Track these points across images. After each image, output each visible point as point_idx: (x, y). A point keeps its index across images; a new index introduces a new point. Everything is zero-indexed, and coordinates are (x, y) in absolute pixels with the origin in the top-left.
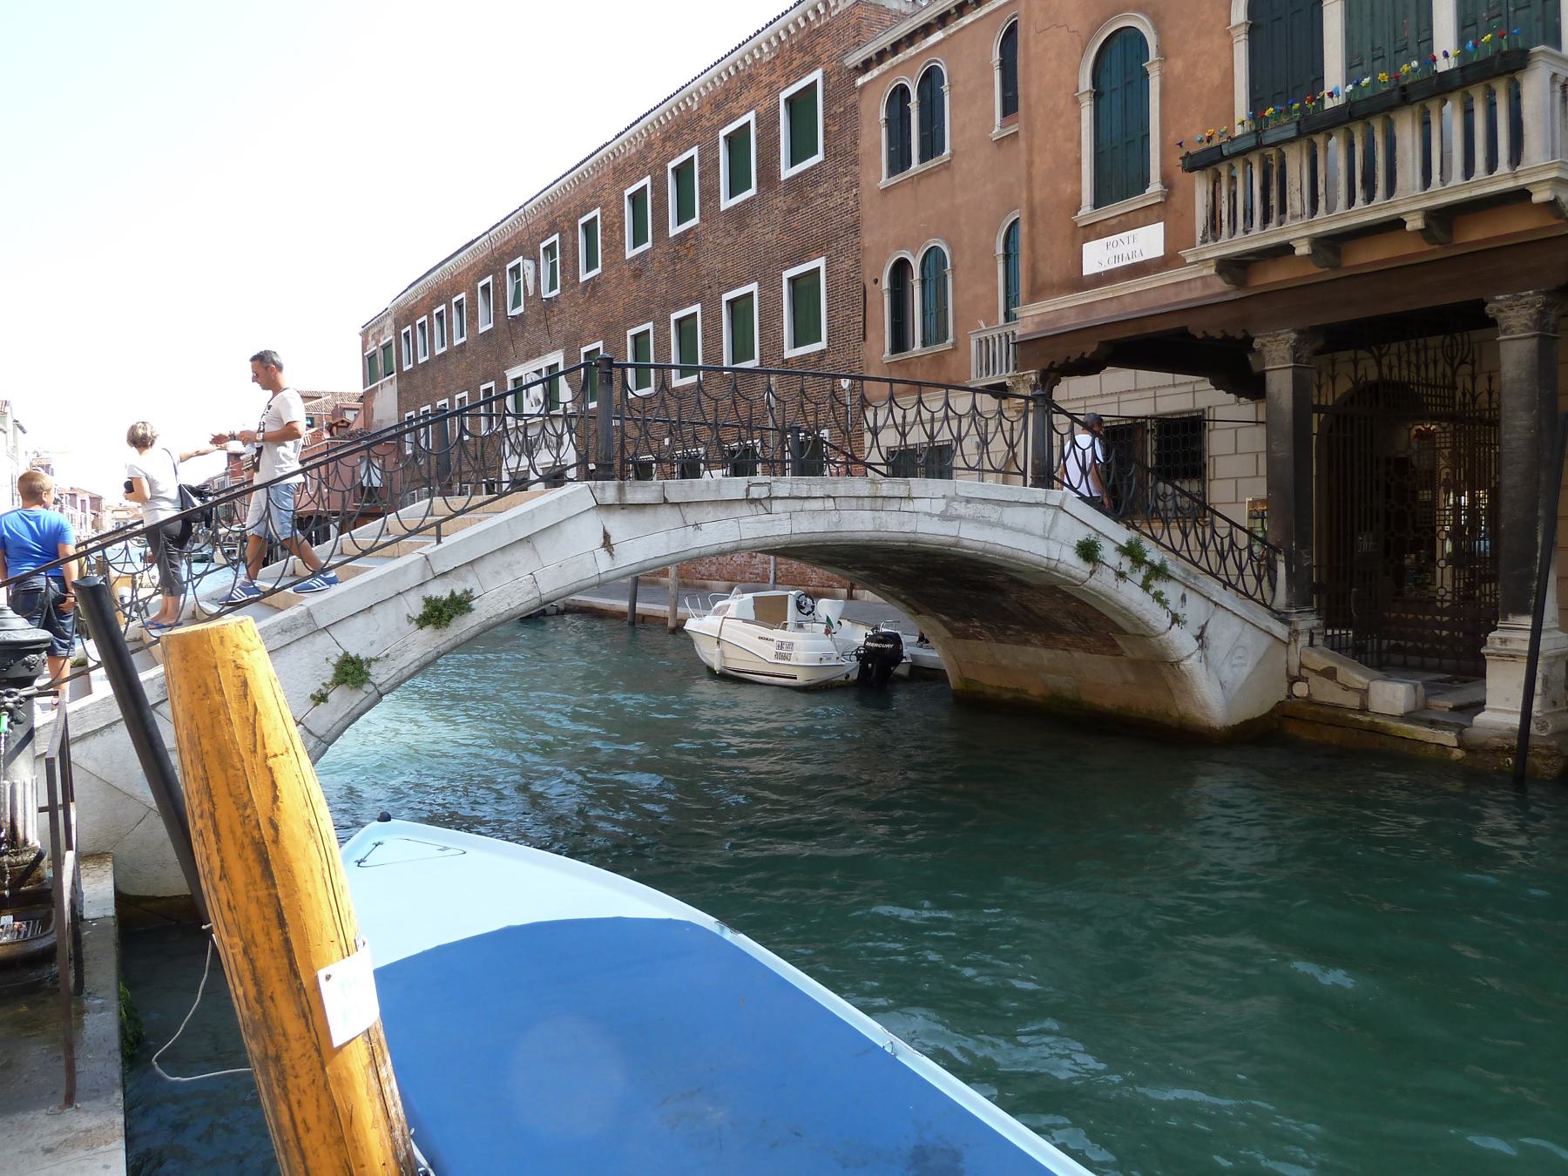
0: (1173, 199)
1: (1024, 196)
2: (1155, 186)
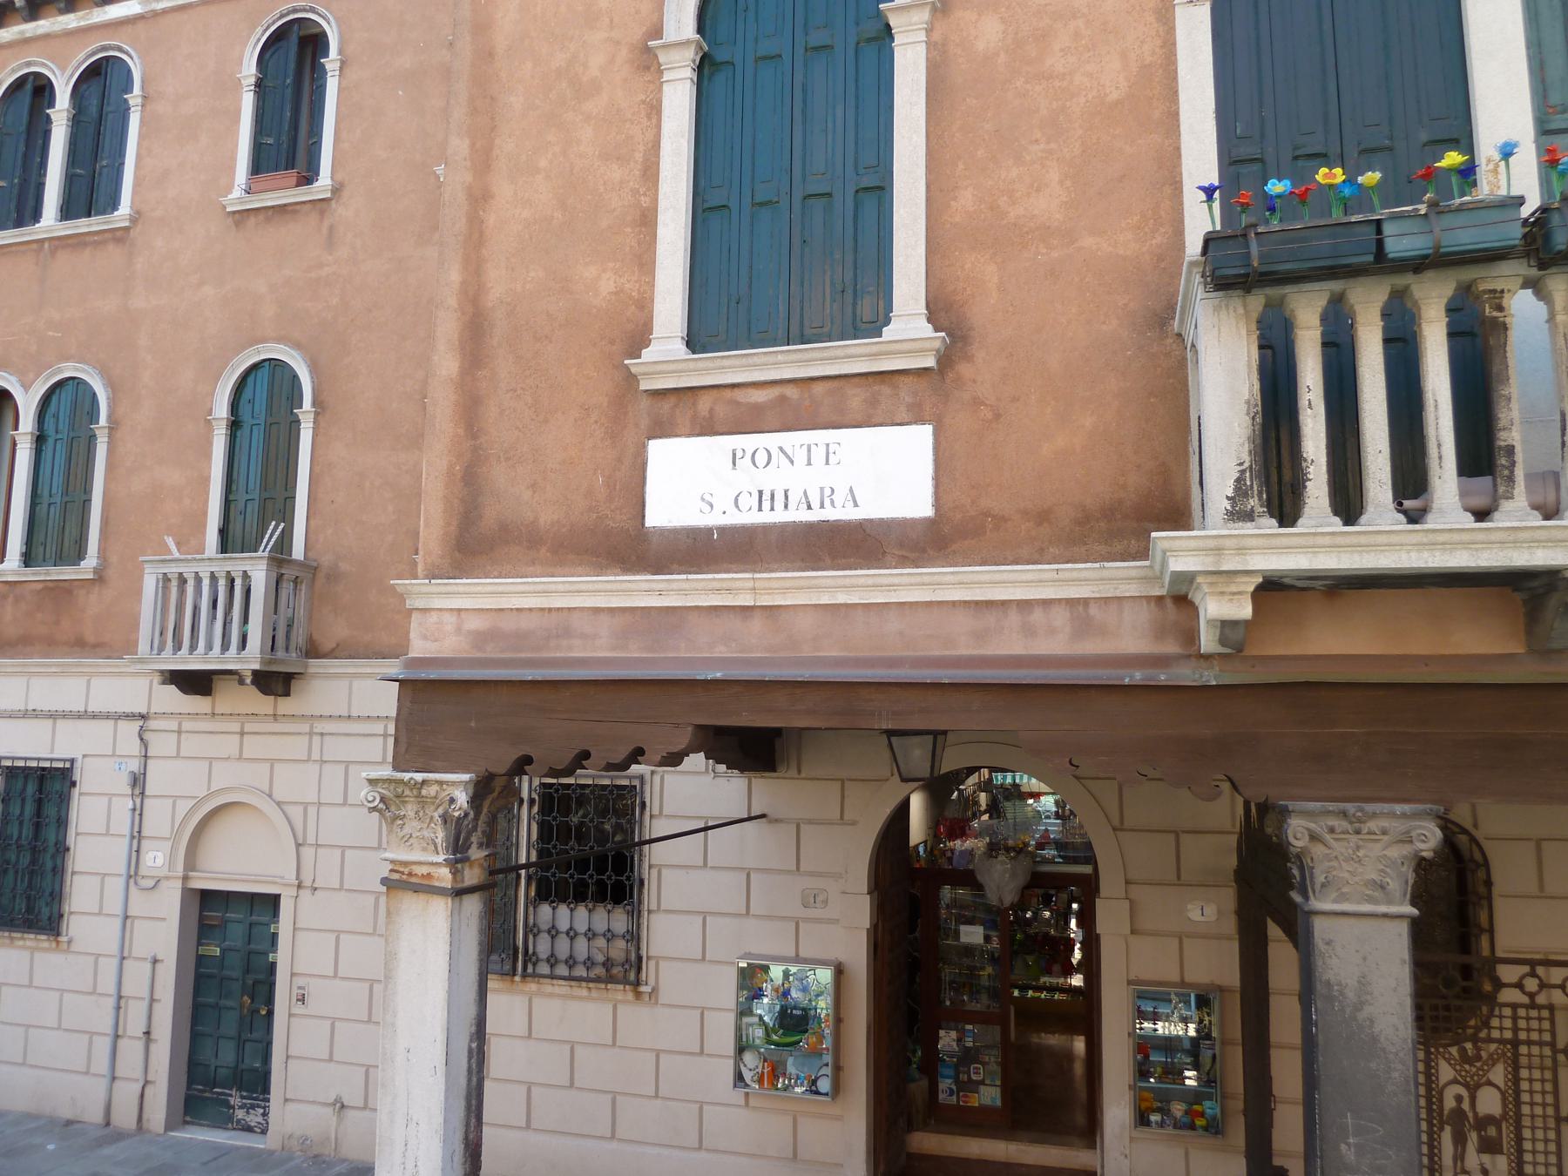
0: (964, 369)
1: (455, 276)
2: (909, 327)
